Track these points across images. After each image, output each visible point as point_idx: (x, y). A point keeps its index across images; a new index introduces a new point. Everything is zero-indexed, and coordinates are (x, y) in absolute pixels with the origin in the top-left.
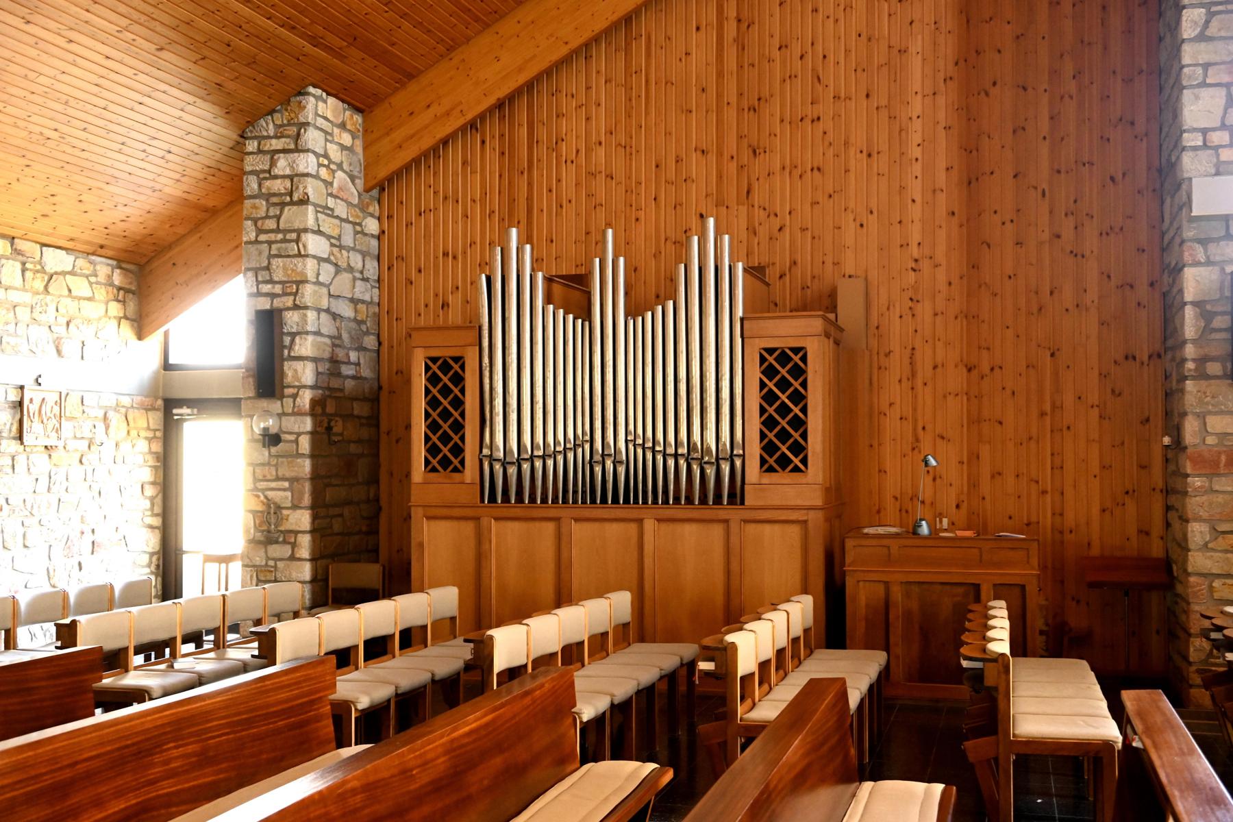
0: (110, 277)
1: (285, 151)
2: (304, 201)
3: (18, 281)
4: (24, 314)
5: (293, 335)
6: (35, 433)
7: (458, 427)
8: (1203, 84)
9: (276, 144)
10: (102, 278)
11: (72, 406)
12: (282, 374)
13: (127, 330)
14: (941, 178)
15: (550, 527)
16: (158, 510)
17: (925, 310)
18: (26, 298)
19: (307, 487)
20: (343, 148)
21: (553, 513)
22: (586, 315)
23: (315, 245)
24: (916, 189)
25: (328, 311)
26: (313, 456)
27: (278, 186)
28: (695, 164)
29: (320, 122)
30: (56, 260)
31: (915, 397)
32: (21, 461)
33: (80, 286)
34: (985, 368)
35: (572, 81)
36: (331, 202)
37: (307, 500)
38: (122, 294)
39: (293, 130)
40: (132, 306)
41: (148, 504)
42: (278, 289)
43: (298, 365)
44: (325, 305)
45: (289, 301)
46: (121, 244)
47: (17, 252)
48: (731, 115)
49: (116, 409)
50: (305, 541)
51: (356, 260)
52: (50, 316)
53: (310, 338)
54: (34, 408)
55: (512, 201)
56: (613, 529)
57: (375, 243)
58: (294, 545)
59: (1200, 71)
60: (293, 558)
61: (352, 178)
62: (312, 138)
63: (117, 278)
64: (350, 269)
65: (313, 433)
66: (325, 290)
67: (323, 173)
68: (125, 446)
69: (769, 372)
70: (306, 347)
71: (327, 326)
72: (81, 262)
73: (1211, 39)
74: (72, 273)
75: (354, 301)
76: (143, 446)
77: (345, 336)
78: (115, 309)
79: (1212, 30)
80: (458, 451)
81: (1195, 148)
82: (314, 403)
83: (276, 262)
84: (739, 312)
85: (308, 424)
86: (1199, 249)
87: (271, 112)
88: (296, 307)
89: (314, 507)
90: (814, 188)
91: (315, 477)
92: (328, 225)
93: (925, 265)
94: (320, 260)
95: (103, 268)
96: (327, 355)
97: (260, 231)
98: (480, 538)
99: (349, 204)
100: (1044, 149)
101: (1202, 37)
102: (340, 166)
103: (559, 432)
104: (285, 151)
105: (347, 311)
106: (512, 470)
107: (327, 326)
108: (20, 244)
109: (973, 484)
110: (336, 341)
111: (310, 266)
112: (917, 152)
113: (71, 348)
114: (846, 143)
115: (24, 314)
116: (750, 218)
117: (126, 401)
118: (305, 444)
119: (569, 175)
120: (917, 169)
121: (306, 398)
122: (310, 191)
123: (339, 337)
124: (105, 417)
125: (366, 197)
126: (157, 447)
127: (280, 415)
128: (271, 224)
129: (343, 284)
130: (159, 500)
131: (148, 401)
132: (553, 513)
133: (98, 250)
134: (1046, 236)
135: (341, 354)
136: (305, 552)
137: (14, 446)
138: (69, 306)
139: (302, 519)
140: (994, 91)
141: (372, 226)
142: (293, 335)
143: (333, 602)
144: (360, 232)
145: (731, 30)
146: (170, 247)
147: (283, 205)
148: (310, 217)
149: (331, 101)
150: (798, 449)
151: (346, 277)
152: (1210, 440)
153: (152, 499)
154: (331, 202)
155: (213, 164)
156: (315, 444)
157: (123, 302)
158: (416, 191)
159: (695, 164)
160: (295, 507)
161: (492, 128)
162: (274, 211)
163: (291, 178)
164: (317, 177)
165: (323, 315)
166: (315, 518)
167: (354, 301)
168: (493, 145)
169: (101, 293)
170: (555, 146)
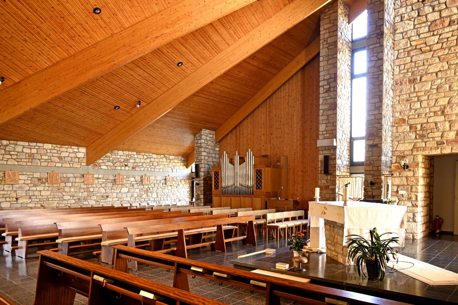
0: (181, 159)
1: (200, 139)
2: (202, 147)
3: (165, 161)
4: (166, 166)
5: (201, 168)
6: (168, 183)
7: (218, 182)
8: (322, 123)
9: (198, 138)
10: (180, 159)
11: (175, 179)
12: (199, 174)
13: (185, 167)
14: (299, 138)
15: (229, 198)
16: (191, 195)
17: (296, 161)
18: (167, 163)
19: (203, 191)
20: (210, 137)
21: (229, 196)
22: (234, 165)
23: (203, 154)
24: (295, 140)
25: (207, 164)
26: (204, 187)
27: (199, 145)
28: (263, 137)
29: (205, 134)
30: (171, 157)
31: (294, 176)
32: (166, 187)
33: (176, 161)
34: (305, 172)
35: (245, 123)
36: (207, 147)
37: (202, 193)
38: (183, 161)
39: (200, 136)
40: (185, 163)
41: (189, 194)
42: (199, 161)
43: (201, 173)
44: (206, 163)
45: (200, 163)
46: (182, 154)
47: (165, 157)
48: (268, 128)
49: (183, 179)
50: (202, 200)
51: (214, 155)
52: (171, 166)
53: (203, 168)
54: (168, 180)
55: (237, 144)
56: (237, 198)
57: (218, 152)
58: (201, 200)
59: (322, 121)
60: (201, 202)
61: (212, 142)
62: (203, 137)
63: (183, 159)
64: (212, 157)
65: (204, 183)
66: (206, 161)
67: (206, 142)
68: (185, 185)
69: (257, 174)
70: (202, 170)
71: (207, 166)
72: (176, 157)
73: (324, 115)
74: (174, 159)
75: (213, 162)
76: (188, 185)
77: (211, 168)
78: (182, 164)
79: (324, 114)
80: (218, 186)
81: (321, 134)
82: (204, 178)
83: (199, 157)
84: (253, 164)
85: (203, 182)
86: (321, 152)
87: (198, 133)
88: (201, 164)
89: (204, 195)
90: (280, 140)
91: (204, 190)
92: (207, 150)
93: (296, 153)
94: (205, 156)
95: (180, 158)
96: (207, 171)
97: (197, 152)
98: (221, 199)
99: (212, 146)
100: (314, 132)
101: (322, 115)
102: (210, 140)
103: (231, 183)
104: (200, 139)
105: (211, 163)
106: (225, 189)
107: (207, 166)
108: (166, 155)
109: (303, 192)
110: (209, 168)
111: (203, 157)
112: (295, 133)
113: (174, 170)
114: (285, 132)
115: (166, 166)
116: (270, 146)
117: (184, 178)
118: (202, 185)
119: (245, 139)
120: (295, 136)
121: (202, 177)
122: (203, 145)
123: (210, 168)
124: (181, 181)
125: (216, 145)
126: (191, 185)
127: (199, 181)
128: (198, 151)
129: (211, 159)
130: (191, 194)
131: (189, 178)
132: (229, 196)
133: (178, 155)
134: (314, 148)
135: (210, 170)
136: (202, 202)
137: (165, 185)
138: (174, 164)
139: (202, 196)
140: (307, 122)
141: (217, 149)
142: (201, 168)
143: (291, 220)
144: (214, 150)
145: (268, 113)
146: (190, 154)
147: (199, 148)
148: (203, 149)
149: (207, 130)
150: (261, 186)
151: (211, 158)
152: (322, 184)
153: (190, 194)
154: (207, 147)
155: (372, 77)
156: (204, 185)
157: (184, 163)
158: (224, 143)
159: (263, 137)
160: (201, 195)
161: (234, 132)
162: (198, 149)
163: (200, 143)
164: (204, 143)
165: (206, 165)
166: (204, 196)
167: (213, 162)
168: (234, 135)
169: (180, 162)
170: (243, 135)
